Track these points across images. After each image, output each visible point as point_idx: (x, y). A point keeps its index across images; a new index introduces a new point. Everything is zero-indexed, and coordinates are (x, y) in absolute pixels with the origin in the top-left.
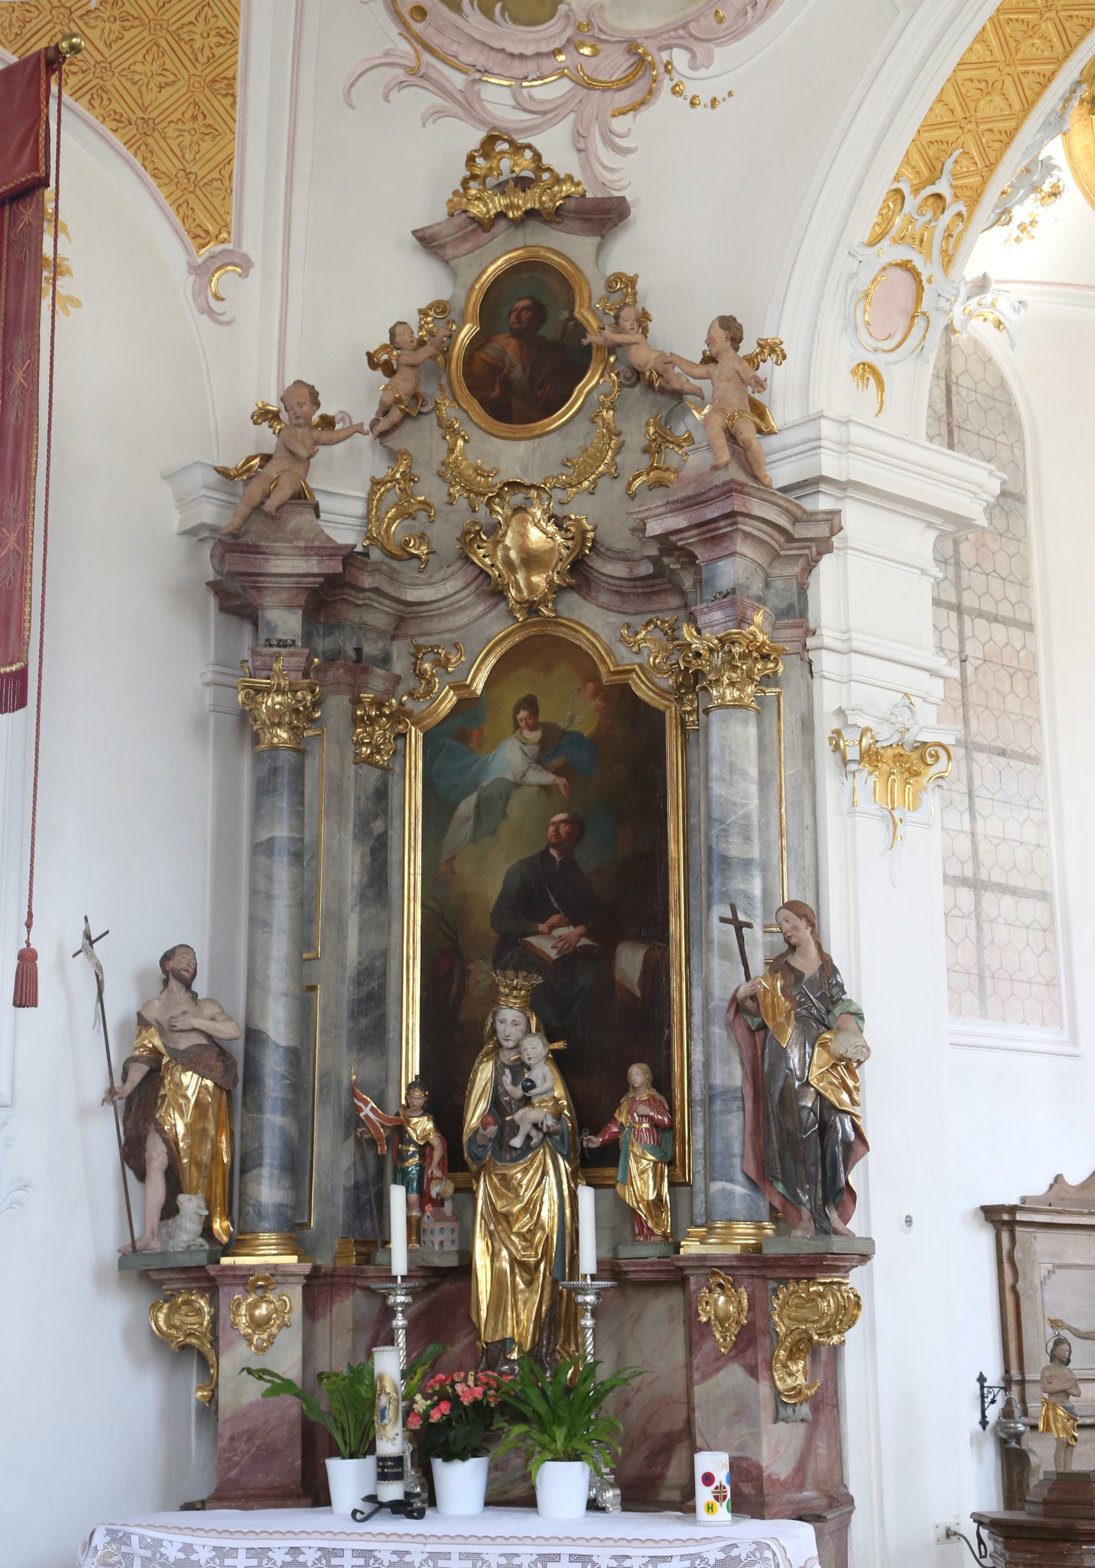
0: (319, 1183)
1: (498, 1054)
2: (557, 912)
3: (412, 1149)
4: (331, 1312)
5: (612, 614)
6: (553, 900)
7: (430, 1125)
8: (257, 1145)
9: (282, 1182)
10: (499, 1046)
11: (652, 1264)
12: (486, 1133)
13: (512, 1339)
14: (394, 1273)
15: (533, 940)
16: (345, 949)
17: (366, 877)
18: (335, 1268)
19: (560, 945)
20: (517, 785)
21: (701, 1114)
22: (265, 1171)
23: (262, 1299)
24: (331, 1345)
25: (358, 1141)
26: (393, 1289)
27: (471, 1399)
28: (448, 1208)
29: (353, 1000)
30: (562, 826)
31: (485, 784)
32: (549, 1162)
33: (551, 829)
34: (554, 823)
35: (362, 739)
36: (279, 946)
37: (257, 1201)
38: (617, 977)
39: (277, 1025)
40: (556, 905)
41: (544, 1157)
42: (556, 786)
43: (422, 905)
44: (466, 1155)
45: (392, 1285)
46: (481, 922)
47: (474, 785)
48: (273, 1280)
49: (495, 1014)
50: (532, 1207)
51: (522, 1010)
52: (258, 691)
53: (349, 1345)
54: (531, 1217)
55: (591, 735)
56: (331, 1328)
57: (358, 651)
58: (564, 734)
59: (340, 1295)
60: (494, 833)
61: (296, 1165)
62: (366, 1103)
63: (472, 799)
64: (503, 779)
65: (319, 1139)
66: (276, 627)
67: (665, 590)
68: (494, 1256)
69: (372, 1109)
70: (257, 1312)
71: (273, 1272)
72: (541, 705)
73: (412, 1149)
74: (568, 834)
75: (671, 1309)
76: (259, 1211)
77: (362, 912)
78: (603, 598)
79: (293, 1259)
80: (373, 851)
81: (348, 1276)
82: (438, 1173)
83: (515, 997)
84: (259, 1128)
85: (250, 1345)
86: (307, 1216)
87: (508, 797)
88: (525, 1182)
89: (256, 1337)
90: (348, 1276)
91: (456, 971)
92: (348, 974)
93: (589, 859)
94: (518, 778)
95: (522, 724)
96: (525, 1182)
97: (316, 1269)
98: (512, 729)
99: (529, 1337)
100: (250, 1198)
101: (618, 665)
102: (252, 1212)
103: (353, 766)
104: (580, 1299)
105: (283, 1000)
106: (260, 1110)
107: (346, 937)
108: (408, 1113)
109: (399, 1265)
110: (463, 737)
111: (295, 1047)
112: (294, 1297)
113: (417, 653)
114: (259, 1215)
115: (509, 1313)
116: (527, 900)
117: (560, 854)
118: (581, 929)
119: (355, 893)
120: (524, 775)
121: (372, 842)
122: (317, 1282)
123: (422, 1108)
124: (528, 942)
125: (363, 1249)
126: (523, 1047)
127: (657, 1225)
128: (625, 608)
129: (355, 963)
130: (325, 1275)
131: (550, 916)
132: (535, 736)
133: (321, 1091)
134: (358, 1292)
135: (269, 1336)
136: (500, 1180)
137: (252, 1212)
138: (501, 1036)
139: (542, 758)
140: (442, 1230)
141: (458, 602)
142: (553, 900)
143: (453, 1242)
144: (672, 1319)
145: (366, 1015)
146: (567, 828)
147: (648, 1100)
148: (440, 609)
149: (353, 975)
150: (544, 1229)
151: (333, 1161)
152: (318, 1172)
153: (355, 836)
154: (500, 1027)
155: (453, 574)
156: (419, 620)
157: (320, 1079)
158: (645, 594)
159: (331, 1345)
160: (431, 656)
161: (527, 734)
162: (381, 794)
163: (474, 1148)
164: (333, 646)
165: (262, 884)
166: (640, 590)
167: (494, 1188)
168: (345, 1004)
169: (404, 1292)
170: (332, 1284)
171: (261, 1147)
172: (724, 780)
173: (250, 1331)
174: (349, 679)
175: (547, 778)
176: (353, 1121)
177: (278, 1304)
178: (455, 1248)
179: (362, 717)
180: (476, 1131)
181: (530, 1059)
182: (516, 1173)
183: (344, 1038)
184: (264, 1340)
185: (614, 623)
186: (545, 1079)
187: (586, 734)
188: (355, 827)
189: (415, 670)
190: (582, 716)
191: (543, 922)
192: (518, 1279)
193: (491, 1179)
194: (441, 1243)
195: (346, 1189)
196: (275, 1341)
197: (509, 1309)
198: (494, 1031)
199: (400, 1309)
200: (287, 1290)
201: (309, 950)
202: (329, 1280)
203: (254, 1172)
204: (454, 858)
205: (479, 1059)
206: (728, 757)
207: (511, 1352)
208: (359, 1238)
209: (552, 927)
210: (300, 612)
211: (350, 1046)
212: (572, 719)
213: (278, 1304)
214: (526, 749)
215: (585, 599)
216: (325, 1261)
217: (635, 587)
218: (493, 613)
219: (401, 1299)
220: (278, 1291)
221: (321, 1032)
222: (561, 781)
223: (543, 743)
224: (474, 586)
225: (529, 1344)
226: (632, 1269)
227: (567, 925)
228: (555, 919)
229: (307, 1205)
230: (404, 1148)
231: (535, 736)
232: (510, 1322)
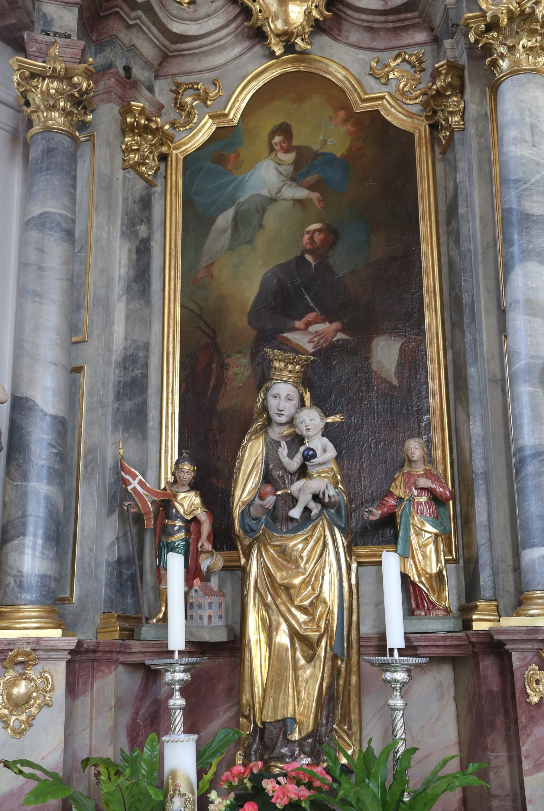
0: (82, 558)
1: (266, 432)
2: (312, 310)
3: (179, 523)
4: (92, 689)
5: (361, 51)
6: (309, 299)
7: (197, 501)
8: (20, 513)
9: (47, 552)
10: (269, 421)
11: (444, 639)
12: (264, 503)
13: (294, 719)
14: (170, 648)
15: (289, 335)
16: (111, 334)
17: (132, 272)
18: (98, 643)
19: (316, 339)
20: (273, 200)
21: (483, 487)
22: (29, 540)
23: (23, 676)
24: (91, 722)
25: (123, 517)
26: (170, 664)
27: (285, 801)
28: (214, 583)
29: (119, 383)
30: (316, 235)
31: (242, 199)
32: (328, 533)
33: (306, 237)
34: (308, 232)
35: (131, 146)
36: (50, 316)
37: (19, 571)
38: (374, 367)
39: (46, 394)
40: (311, 304)
41: (322, 529)
42: (311, 200)
43: (182, 306)
44: (237, 527)
45: (168, 661)
46: (239, 320)
47: (232, 200)
48: (34, 655)
49: (267, 390)
50: (314, 579)
51: (295, 385)
52: (33, 75)
53: (110, 723)
54: (313, 589)
55: (342, 155)
56: (92, 705)
57: (127, 70)
58: (316, 155)
59: (102, 671)
60: (250, 242)
61: (60, 536)
62: (134, 477)
63: (230, 213)
64: (259, 195)
65: (83, 514)
66: (52, 21)
67: (414, 26)
68: (270, 630)
69: (140, 483)
70: (15, 691)
71: (34, 646)
72: (294, 131)
73: (179, 523)
74: (323, 241)
75: (440, 685)
76: (21, 581)
77: (128, 302)
78: (354, 36)
79: (57, 633)
80: (138, 251)
81: (111, 652)
82: (208, 546)
83: (290, 372)
84: (23, 496)
85: (6, 728)
86: (68, 590)
87: (264, 210)
88: (305, 554)
89: (14, 718)
90: (111, 652)
91: (214, 365)
92: (114, 358)
93: (343, 263)
94: (273, 194)
95: (277, 148)
96: (305, 554)
97: (80, 643)
98: (267, 152)
99: (312, 717)
100: (11, 568)
101: (366, 94)
102: (12, 582)
103: (121, 171)
104: (388, 676)
105: (53, 368)
106: (25, 478)
107: (113, 324)
108: (175, 488)
109: (177, 640)
110: (220, 160)
111: (62, 417)
112: (58, 672)
113: (177, 90)
114: (20, 586)
115: (290, 690)
116: (282, 302)
117: (315, 259)
118: (336, 325)
119: (122, 284)
120: (279, 191)
121: (137, 243)
122: (78, 657)
123: (189, 484)
124: (286, 338)
125: (126, 625)
126: (297, 421)
127: (439, 598)
128: (374, 45)
129: (121, 348)
130: (87, 651)
131: (307, 313)
132: (290, 157)
133: (86, 467)
134: (121, 668)
135: (28, 717)
136: (276, 551)
137: (12, 582)
138: (273, 412)
139: (296, 177)
140: (210, 604)
141: (218, 41)
142: (309, 299)
143: (220, 617)
144: (442, 696)
145: (130, 399)
146: (322, 236)
147: (425, 473)
148: (201, 47)
149: (119, 359)
150: (325, 602)
151: (98, 535)
152: (82, 547)
153: (123, 233)
154: (272, 403)
155: (215, 12)
156: (180, 60)
157: (85, 455)
158: (396, 29)
159: (91, 722)
160: (191, 92)
161: (281, 156)
162: (146, 203)
163: (248, 521)
164: (104, 61)
165: (33, 256)
166: (391, 25)
167: (273, 560)
168: (111, 386)
169: (182, 668)
170: (94, 660)
171: (24, 515)
172: (525, 141)
173: (6, 712)
174: (119, 90)
175: (302, 193)
176: (118, 495)
177: (38, 681)
178: (221, 623)
179: (132, 124)
180: (249, 504)
181: (308, 430)
182: (296, 543)
183: (110, 418)
184: (22, 722)
185: (363, 59)
186: (325, 451)
187: (338, 155)
188: (122, 224)
189: (176, 104)
190: (333, 139)
191: (299, 319)
192: (298, 654)
193: (267, 551)
194: (210, 618)
195: (109, 564)
196: (34, 722)
197: (290, 685)
198: (265, 409)
199: (177, 687)
200: (50, 666)
201: (76, 334)
202: (91, 655)
203: (16, 542)
204: (212, 264)
205: (247, 436)
206: (528, 120)
207: (292, 733)
208: (121, 614)
209: (308, 324)
210: (76, 10)
211: (115, 426)
212: (325, 142)
213: (38, 681)
214: (281, 169)
215: (336, 39)
216: (88, 636)
217: (387, 22)
218: (249, 55)
219: (180, 676)
220: (39, 667)
221: (87, 411)
222: (315, 196)
223: (297, 164)
224: (233, 26)
225: (311, 724)
226: (423, 644)
227: (323, 321)
228: (310, 316)
229: (69, 579)
230: (170, 522)
231: (290, 157)
232: (291, 700)
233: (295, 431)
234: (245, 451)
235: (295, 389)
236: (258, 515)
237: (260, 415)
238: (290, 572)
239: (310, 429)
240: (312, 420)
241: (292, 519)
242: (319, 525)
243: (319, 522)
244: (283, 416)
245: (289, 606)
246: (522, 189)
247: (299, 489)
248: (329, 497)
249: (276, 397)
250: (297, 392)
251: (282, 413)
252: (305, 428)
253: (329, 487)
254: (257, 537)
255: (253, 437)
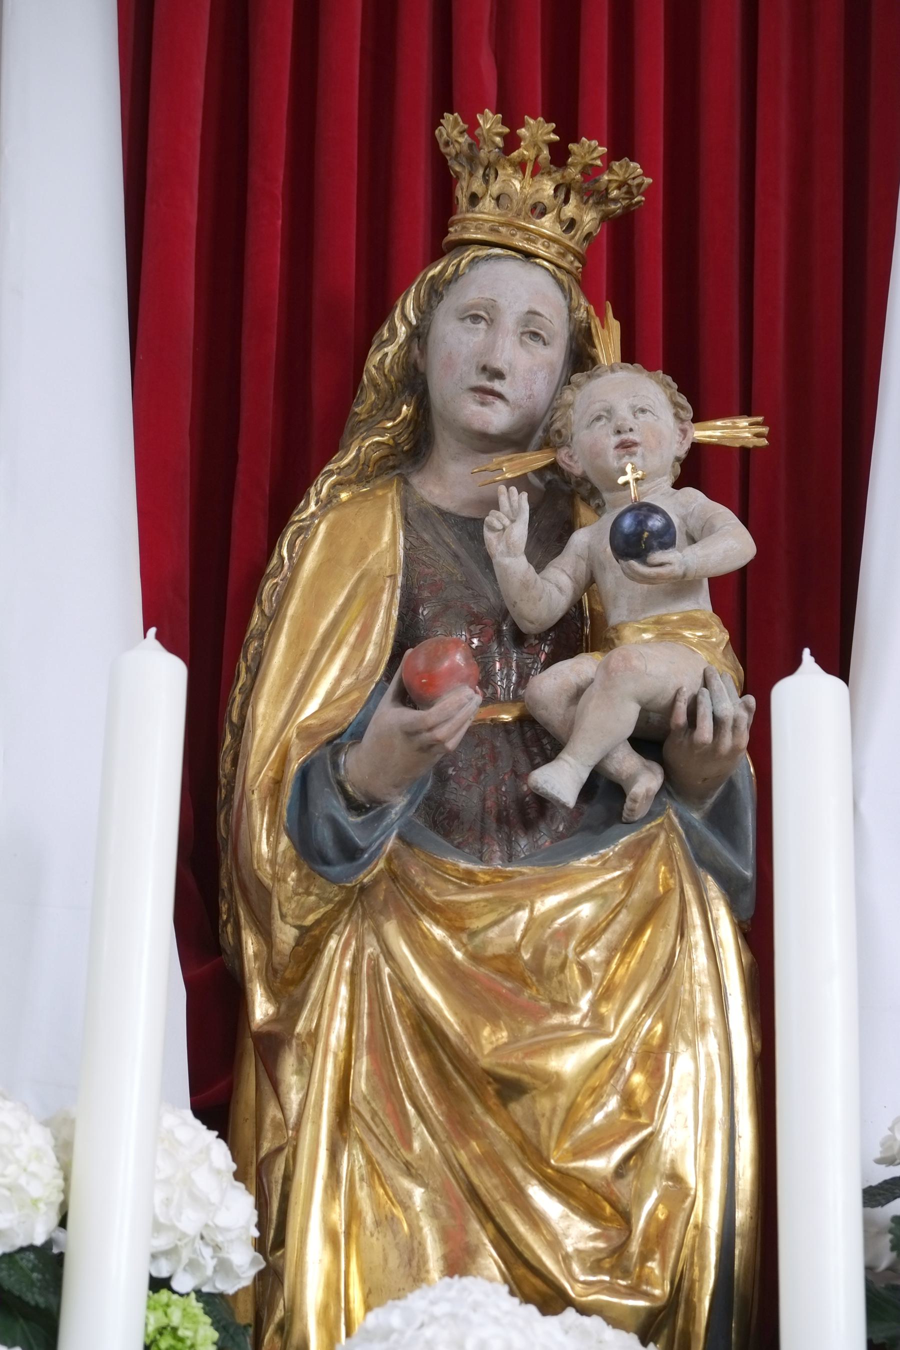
32: (690, 893)
49: (436, 292)
138: (450, 388)
154: (456, 344)
180: (337, 741)
198: (414, 381)
233: (554, 467)
234: (306, 546)
235: (559, 295)
236: (379, 788)
237: (387, 406)
238: (529, 1028)
239: (635, 444)
240: (638, 423)
241: (543, 804)
242: (655, 852)
243: (656, 837)
244: (499, 404)
245: (518, 1172)
246: (428, 781)
247: (573, 691)
248: (718, 723)
249: (476, 318)
250: (565, 312)
251: (497, 385)
252: (615, 440)
253: (717, 683)
254: (363, 890)
255: (344, 496)
